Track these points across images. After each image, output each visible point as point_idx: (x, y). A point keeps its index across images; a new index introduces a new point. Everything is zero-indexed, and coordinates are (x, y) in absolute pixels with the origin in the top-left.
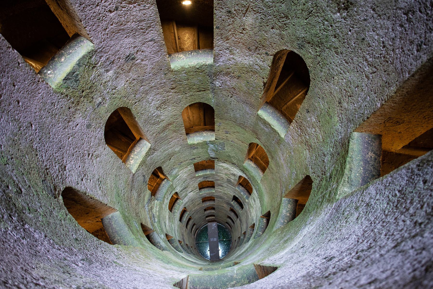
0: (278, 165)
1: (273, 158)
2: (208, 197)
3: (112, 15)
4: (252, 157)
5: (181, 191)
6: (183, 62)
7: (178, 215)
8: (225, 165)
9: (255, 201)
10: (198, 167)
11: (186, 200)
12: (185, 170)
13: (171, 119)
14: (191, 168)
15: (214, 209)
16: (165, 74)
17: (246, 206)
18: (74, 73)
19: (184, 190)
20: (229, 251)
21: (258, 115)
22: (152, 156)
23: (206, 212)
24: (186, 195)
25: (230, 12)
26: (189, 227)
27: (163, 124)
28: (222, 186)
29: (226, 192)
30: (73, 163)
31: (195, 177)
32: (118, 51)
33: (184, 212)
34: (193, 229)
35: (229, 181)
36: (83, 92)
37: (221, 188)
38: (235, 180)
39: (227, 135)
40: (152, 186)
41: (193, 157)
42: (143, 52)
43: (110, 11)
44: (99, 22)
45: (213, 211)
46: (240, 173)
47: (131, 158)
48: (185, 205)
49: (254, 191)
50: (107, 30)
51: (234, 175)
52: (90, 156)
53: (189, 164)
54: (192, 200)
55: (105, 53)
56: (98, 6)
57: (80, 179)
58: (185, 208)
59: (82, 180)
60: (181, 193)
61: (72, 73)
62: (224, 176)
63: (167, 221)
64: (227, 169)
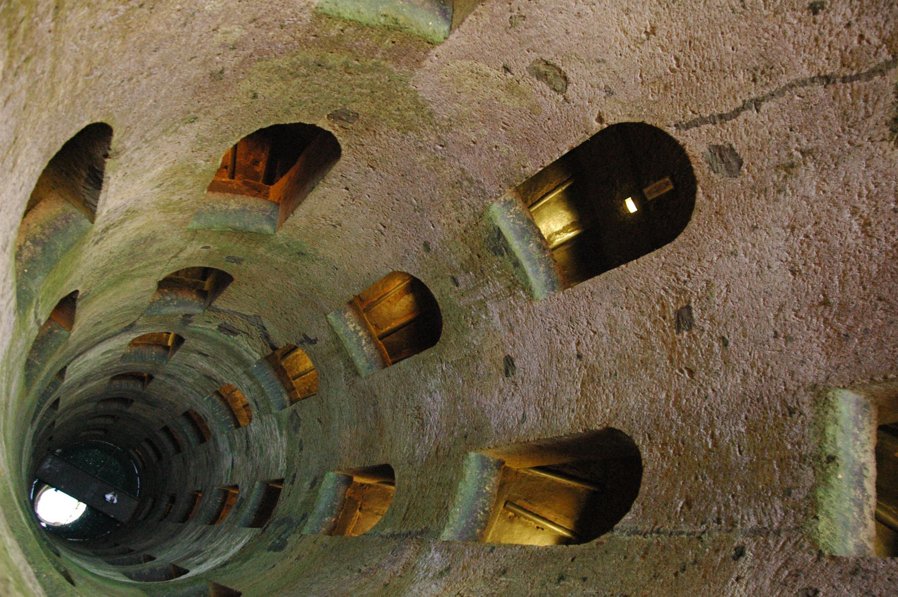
2: (195, 418)
3: (573, 345)
13: (388, 437)
16: (466, 437)
18: (506, 250)
19: (245, 444)
22: (343, 374)
25: (504, 572)
27: (388, 413)
28: (198, 539)
30: (377, 184)
32: (524, 345)
36: (479, 256)
37: (195, 538)
40: (294, 379)
42: (513, 394)
43: (578, 344)
44: (567, 318)
46: (193, 572)
47: (358, 328)
50: (555, 331)
52: (382, 228)
55: (526, 319)
56: (588, 323)
57: (349, 184)
59: (347, 189)
60: (244, 436)
61: (508, 249)
63: (207, 366)
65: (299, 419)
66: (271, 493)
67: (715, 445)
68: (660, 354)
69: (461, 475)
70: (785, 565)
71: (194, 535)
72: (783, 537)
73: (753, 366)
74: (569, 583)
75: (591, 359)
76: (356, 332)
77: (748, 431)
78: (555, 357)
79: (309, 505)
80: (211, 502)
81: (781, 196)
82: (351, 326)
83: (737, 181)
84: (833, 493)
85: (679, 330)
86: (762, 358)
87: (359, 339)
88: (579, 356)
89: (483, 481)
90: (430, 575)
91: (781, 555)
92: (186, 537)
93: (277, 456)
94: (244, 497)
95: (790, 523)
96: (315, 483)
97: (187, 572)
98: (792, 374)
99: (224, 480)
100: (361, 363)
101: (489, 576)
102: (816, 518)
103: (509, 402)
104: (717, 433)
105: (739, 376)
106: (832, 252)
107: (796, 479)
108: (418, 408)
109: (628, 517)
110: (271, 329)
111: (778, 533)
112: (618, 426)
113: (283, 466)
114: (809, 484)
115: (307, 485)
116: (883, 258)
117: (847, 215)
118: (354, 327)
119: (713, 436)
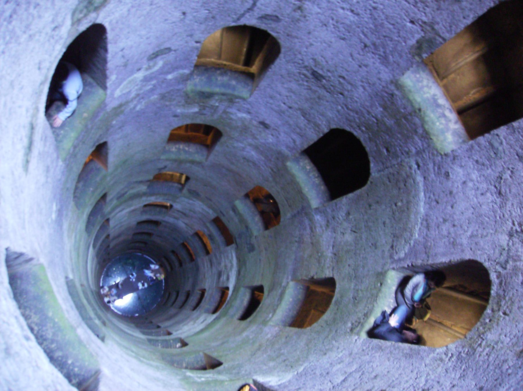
0: (243, 330)
1: (250, 322)
4: (313, 292)
5: (178, 211)
6: (424, 90)
7: (145, 217)
8: (235, 261)
9: (202, 323)
10: (217, 222)
11: (171, 220)
12: (205, 207)
14: (212, 215)
15: (181, 265)
17: (196, 313)
20: (128, 316)
21: (386, 272)
23: (171, 254)
24: (177, 219)
26: (139, 237)
27: (233, 167)
28: (211, 265)
29: (206, 275)
31: (205, 224)
33: (156, 223)
34: (137, 244)
35: (220, 275)
37: (209, 266)
38: (223, 283)
39: (264, 250)
41: (225, 213)
45: (177, 264)
46: (231, 286)
47: (177, 146)
48: (164, 221)
49: (215, 316)
51: (228, 279)
53: (215, 211)
54: (175, 229)
58: (160, 223)
62: (223, 264)
64: (232, 266)
65: (195, 191)
66: (218, 222)
67: (377, 120)
68: (322, 92)
69: (293, 176)
70: (434, 165)
71: (207, 264)
72: (426, 151)
73: (362, 82)
74: (374, 207)
75: (296, 106)
76: (179, 149)
77: (383, 109)
78: (281, 113)
79: (242, 220)
80: (195, 245)
81: (307, 18)
82: (174, 149)
83: (283, 22)
84: (430, 123)
85: (320, 81)
86: (363, 77)
87: (184, 150)
88: (290, 108)
89: (304, 168)
90: (324, 228)
91: (431, 161)
92: (204, 268)
93: (203, 209)
94: (209, 233)
95: (425, 145)
96: (234, 209)
97: (228, 288)
98: (379, 79)
99: (189, 231)
100: (198, 157)
101: (345, 218)
102: (431, 139)
103: (280, 137)
104: (373, 115)
105: (361, 88)
106: (350, 26)
107: (414, 124)
108: (245, 158)
109: (372, 165)
110: (140, 179)
111: (424, 151)
112: (334, 127)
113: (211, 212)
114: (420, 125)
115: (231, 213)
116: (370, 20)
117: (341, 11)
118: (176, 148)
119: (373, 117)
